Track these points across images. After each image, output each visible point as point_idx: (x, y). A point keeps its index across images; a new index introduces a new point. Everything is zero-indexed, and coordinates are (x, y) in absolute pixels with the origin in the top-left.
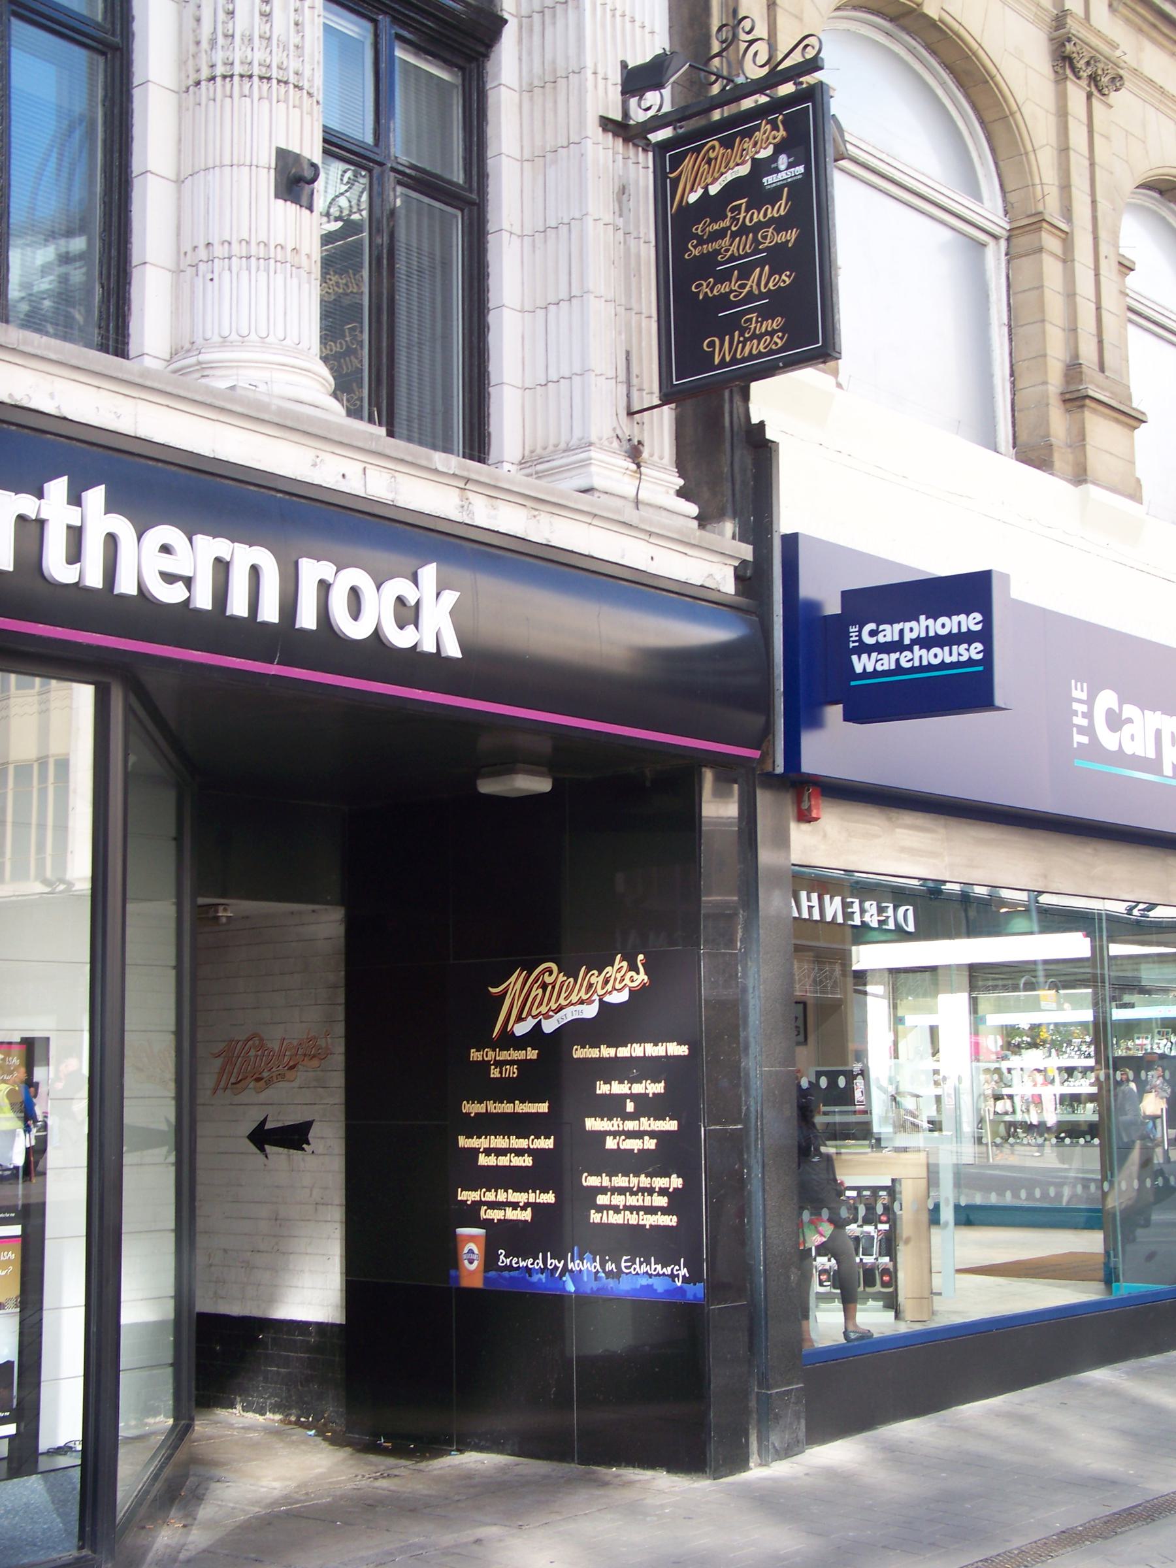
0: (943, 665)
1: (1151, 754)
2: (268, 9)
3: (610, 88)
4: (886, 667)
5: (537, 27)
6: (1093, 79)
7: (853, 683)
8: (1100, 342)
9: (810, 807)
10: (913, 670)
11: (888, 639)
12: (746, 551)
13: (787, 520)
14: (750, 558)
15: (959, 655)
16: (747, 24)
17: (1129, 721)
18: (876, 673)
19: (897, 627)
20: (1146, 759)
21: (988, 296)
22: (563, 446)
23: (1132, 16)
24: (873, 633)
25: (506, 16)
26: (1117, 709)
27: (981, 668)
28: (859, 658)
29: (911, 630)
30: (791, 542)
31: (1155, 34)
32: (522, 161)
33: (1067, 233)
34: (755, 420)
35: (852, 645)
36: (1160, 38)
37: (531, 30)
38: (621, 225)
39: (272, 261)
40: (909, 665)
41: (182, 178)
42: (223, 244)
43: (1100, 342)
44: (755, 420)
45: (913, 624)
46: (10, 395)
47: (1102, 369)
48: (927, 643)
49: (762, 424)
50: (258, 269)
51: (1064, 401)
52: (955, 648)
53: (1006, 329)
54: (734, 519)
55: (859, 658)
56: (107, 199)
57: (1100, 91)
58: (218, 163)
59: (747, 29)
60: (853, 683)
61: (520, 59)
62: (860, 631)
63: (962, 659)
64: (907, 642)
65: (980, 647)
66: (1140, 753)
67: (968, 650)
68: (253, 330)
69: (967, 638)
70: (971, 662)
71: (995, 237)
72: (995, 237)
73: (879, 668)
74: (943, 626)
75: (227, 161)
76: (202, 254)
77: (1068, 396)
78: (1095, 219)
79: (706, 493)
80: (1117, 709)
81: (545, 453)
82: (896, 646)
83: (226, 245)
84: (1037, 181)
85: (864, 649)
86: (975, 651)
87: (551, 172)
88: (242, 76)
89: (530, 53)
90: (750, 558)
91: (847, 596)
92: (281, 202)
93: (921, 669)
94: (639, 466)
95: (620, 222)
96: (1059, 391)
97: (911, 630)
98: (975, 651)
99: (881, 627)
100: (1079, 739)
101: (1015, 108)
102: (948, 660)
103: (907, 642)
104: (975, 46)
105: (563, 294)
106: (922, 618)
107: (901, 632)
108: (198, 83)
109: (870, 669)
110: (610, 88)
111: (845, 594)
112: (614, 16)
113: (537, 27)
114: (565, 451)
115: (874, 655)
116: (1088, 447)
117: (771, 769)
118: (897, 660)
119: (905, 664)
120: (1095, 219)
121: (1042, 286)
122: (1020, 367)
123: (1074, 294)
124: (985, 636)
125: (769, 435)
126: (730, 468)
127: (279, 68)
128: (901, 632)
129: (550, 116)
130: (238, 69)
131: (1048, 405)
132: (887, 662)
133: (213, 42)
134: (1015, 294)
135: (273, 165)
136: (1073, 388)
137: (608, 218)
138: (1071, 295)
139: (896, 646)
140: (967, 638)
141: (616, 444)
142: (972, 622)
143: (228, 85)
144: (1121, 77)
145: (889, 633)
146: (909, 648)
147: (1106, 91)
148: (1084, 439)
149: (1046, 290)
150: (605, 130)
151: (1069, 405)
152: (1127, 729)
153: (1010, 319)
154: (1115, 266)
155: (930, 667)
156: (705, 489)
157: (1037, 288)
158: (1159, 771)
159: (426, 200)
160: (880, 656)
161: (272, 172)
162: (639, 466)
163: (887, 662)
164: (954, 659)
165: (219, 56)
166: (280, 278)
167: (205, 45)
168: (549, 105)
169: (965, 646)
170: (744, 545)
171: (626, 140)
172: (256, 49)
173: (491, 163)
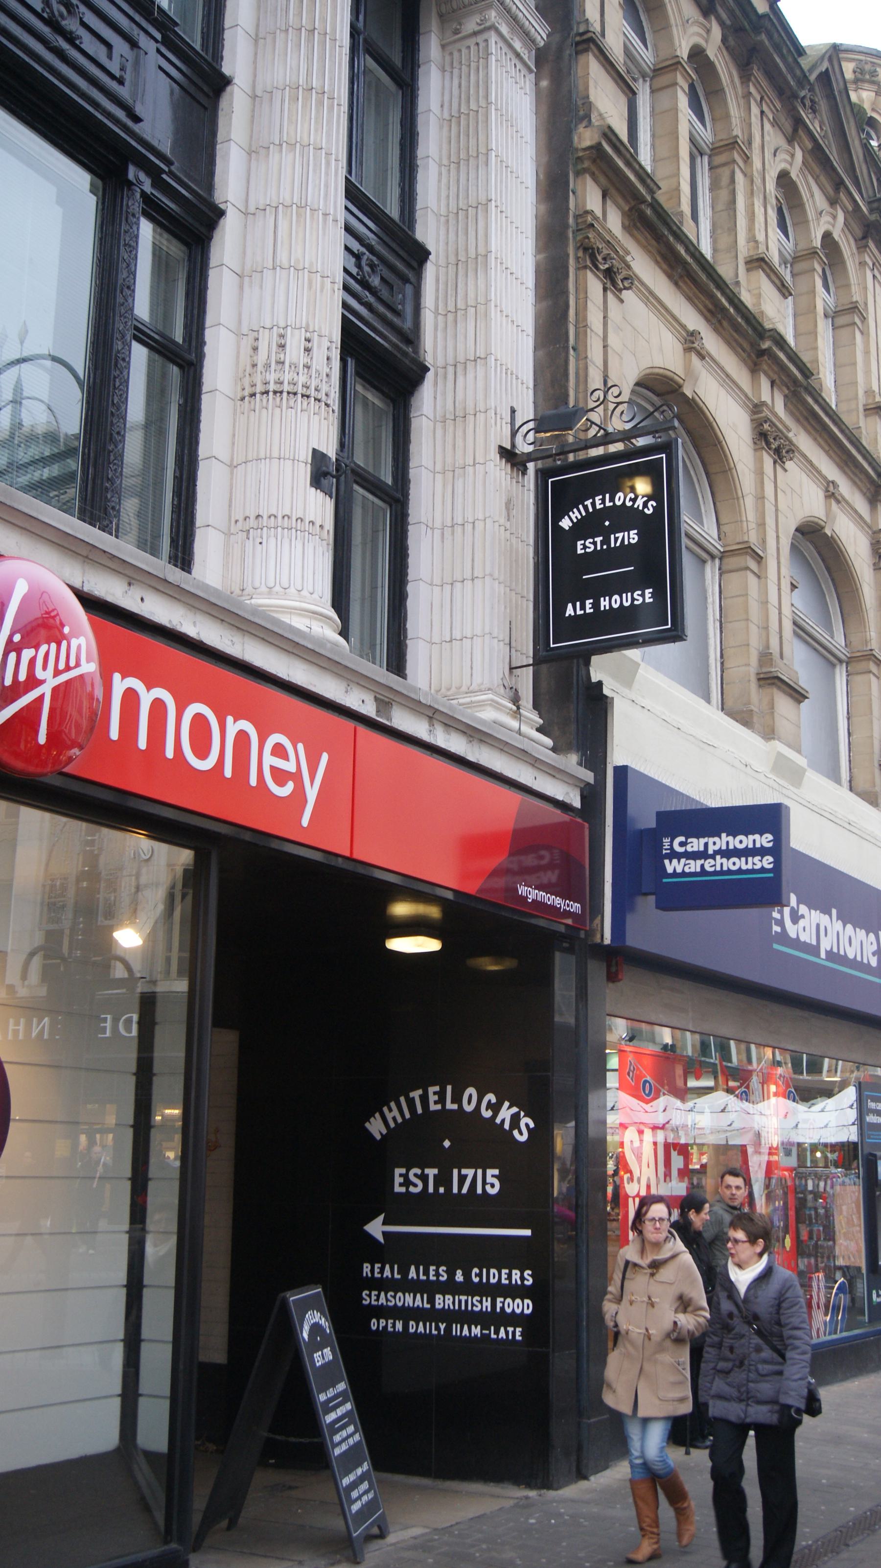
0: (740, 871)
1: (814, 942)
2: (283, 342)
3: (504, 425)
4: (692, 870)
5: (450, 376)
6: (778, 451)
7: (665, 880)
8: (781, 637)
9: (617, 971)
10: (715, 873)
11: (695, 849)
12: (588, 776)
13: (618, 756)
14: (592, 781)
15: (754, 864)
16: (615, 391)
17: (803, 916)
18: (684, 874)
19: (703, 841)
20: (810, 945)
21: (706, 598)
22: (464, 689)
23: (794, 411)
24: (682, 844)
25: (429, 366)
26: (796, 907)
27: (771, 875)
28: (671, 862)
29: (714, 843)
30: (622, 772)
31: (806, 423)
32: (434, 473)
33: (762, 558)
34: (594, 679)
35: (664, 852)
36: (809, 427)
37: (445, 377)
38: (508, 527)
39: (294, 530)
40: (712, 869)
41: (235, 464)
42: (270, 517)
43: (781, 637)
44: (594, 679)
45: (716, 839)
46: (170, 621)
47: (782, 657)
48: (727, 853)
49: (600, 684)
50: (283, 537)
51: (759, 679)
52: (750, 859)
53: (718, 624)
54: (578, 751)
55: (671, 862)
56: (178, 474)
57: (781, 459)
58: (268, 456)
59: (616, 395)
60: (665, 880)
61: (435, 398)
62: (672, 842)
63: (756, 867)
64: (710, 852)
65: (771, 859)
66: (808, 941)
67: (761, 861)
68: (292, 583)
69: (762, 852)
70: (763, 870)
71: (713, 557)
72: (713, 557)
73: (687, 870)
74: (741, 842)
75: (275, 454)
76: (252, 522)
77: (762, 676)
78: (778, 549)
79: (557, 732)
80: (796, 907)
81: (449, 693)
82: (703, 855)
83: (272, 518)
84: (744, 519)
85: (674, 855)
86: (767, 862)
87: (459, 484)
88: (289, 393)
89: (444, 393)
90: (592, 781)
91: (661, 816)
92: (313, 489)
93: (722, 872)
94: (518, 708)
95: (508, 525)
96: (756, 672)
97: (714, 843)
98: (767, 862)
99: (689, 840)
100: (776, 929)
101: (732, 465)
102: (744, 867)
103: (710, 852)
104: (712, 419)
105: (468, 574)
106: (724, 835)
107: (706, 845)
108: (253, 395)
109: (679, 870)
110: (504, 425)
111: (659, 815)
112: (506, 373)
113: (450, 376)
114: (467, 693)
115: (683, 861)
116: (775, 714)
117: (598, 940)
118: (702, 866)
119: (708, 868)
120: (778, 549)
121: (747, 594)
122: (728, 652)
123: (767, 602)
124: (776, 851)
125: (606, 691)
126: (578, 713)
127: (316, 390)
128: (706, 845)
129: (459, 442)
130: (286, 387)
131: (749, 681)
132: (694, 866)
133: (267, 366)
134: (725, 598)
135: (310, 461)
136: (765, 670)
137: (502, 521)
138: (765, 603)
139: (703, 855)
140: (762, 852)
141: (502, 689)
142: (765, 840)
143: (278, 399)
144: (793, 451)
145: (696, 844)
146: (713, 857)
147: (784, 460)
148: (773, 708)
149: (749, 597)
150: (501, 457)
151: (762, 682)
152: (802, 923)
153: (721, 617)
154: (789, 586)
155: (729, 872)
156: (556, 728)
157: (742, 595)
158: (818, 955)
159: (371, 497)
160: (688, 862)
161: (309, 466)
162: (518, 708)
163: (694, 866)
164: (750, 866)
165: (272, 377)
166: (311, 545)
167: (260, 367)
168: (459, 433)
169: (759, 858)
170: (589, 772)
171: (513, 466)
172: (300, 374)
173: (412, 473)
